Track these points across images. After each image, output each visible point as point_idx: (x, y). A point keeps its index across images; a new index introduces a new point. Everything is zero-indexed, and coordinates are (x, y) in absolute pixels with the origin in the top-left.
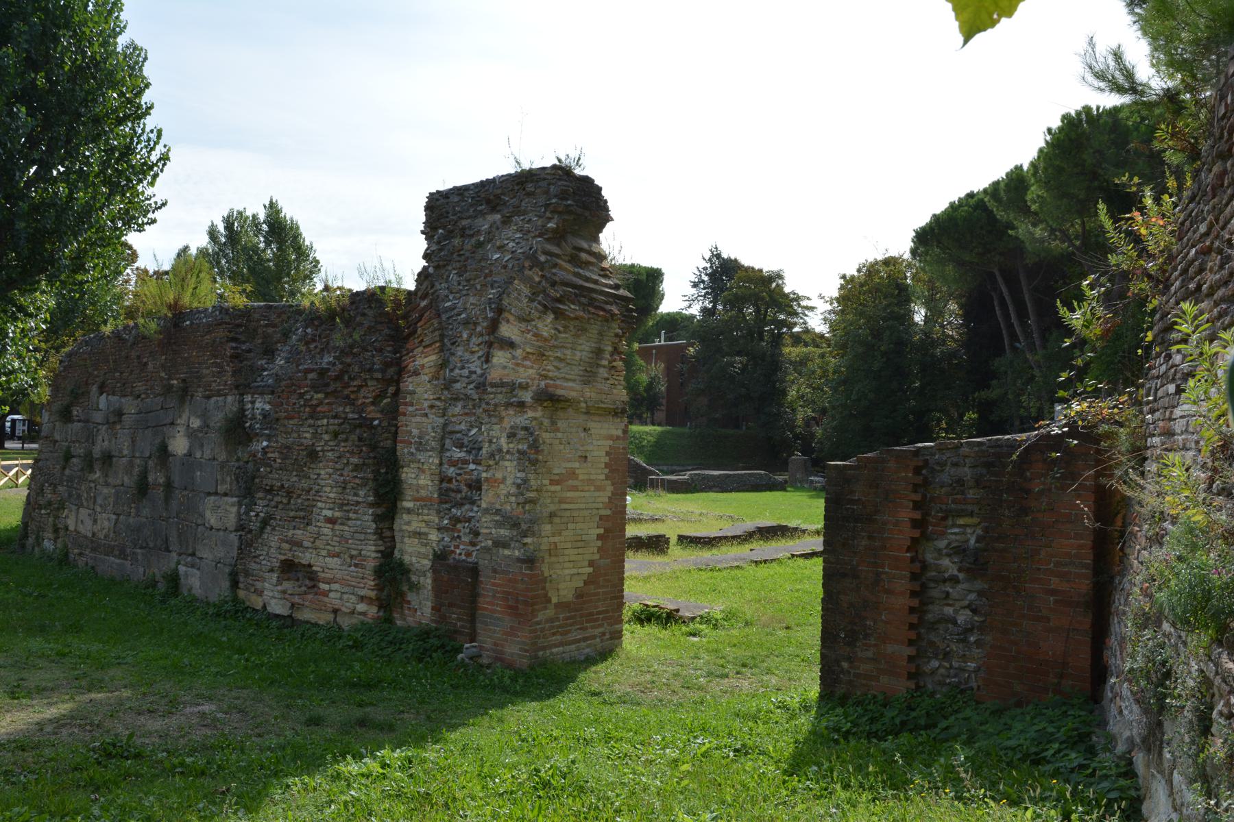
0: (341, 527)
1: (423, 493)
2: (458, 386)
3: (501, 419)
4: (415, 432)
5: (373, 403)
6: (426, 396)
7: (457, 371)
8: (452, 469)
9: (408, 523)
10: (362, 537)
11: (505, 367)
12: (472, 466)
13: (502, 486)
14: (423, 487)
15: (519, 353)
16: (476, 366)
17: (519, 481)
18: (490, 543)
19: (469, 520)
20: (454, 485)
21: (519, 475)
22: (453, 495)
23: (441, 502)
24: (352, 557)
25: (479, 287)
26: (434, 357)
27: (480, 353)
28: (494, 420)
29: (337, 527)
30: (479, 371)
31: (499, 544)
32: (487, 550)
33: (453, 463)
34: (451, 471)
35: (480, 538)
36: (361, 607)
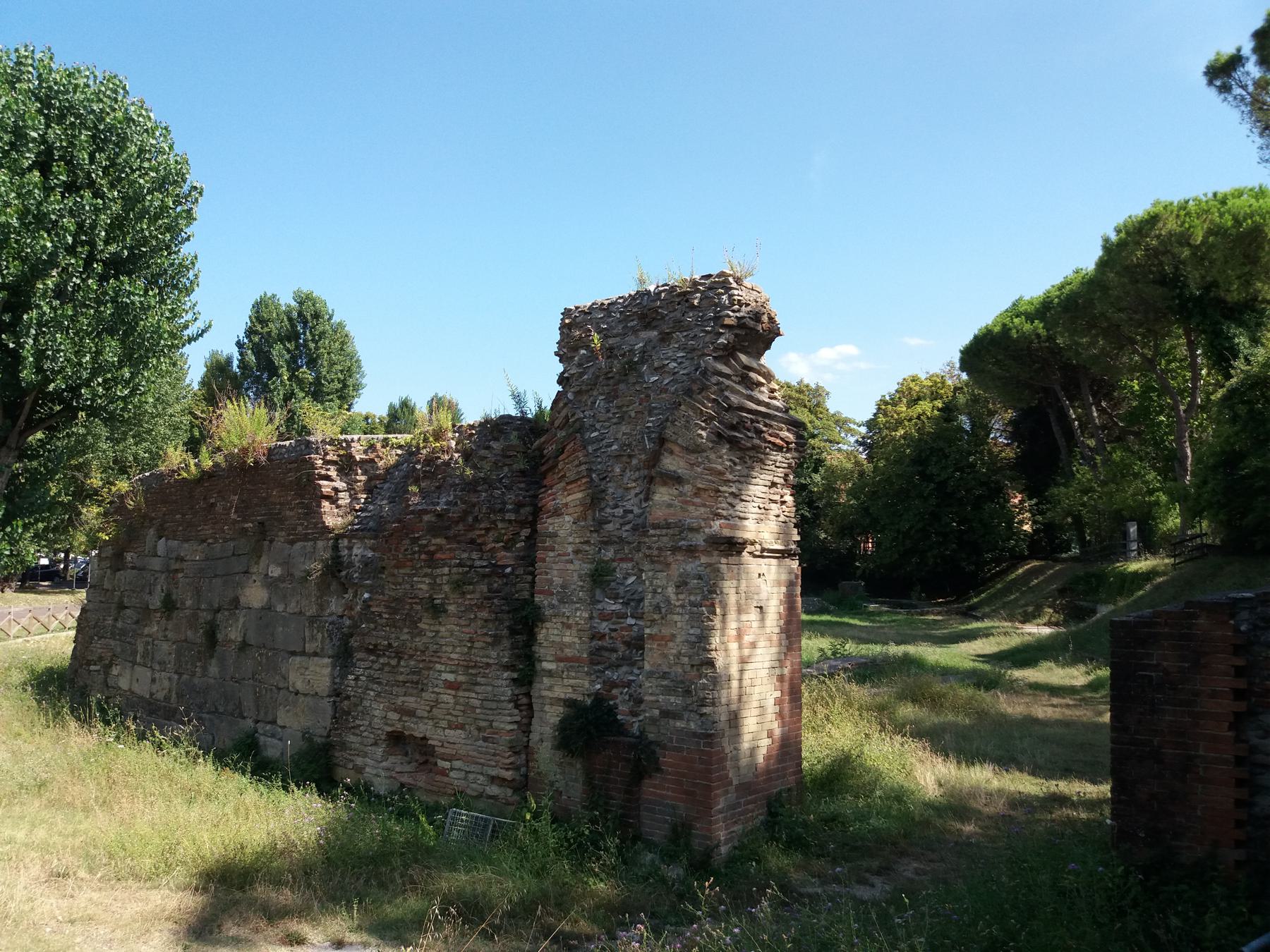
0: (467, 694)
1: (568, 652)
2: (610, 527)
3: (668, 565)
4: (558, 581)
5: (505, 548)
6: (571, 539)
7: (608, 510)
8: (605, 624)
9: (550, 688)
10: (494, 705)
11: (670, 506)
12: (631, 621)
13: (671, 644)
14: (570, 645)
15: (687, 488)
16: (631, 503)
17: (693, 639)
18: (657, 712)
19: (629, 684)
20: (607, 643)
21: (692, 631)
22: (606, 654)
23: (592, 663)
24: (479, 729)
25: (633, 414)
26: (580, 495)
27: (637, 490)
28: (658, 567)
29: (461, 694)
30: (637, 511)
31: (666, 714)
32: (653, 721)
33: (604, 617)
34: (604, 627)
35: (643, 707)
36: (494, 790)
